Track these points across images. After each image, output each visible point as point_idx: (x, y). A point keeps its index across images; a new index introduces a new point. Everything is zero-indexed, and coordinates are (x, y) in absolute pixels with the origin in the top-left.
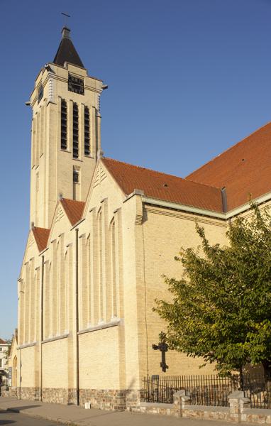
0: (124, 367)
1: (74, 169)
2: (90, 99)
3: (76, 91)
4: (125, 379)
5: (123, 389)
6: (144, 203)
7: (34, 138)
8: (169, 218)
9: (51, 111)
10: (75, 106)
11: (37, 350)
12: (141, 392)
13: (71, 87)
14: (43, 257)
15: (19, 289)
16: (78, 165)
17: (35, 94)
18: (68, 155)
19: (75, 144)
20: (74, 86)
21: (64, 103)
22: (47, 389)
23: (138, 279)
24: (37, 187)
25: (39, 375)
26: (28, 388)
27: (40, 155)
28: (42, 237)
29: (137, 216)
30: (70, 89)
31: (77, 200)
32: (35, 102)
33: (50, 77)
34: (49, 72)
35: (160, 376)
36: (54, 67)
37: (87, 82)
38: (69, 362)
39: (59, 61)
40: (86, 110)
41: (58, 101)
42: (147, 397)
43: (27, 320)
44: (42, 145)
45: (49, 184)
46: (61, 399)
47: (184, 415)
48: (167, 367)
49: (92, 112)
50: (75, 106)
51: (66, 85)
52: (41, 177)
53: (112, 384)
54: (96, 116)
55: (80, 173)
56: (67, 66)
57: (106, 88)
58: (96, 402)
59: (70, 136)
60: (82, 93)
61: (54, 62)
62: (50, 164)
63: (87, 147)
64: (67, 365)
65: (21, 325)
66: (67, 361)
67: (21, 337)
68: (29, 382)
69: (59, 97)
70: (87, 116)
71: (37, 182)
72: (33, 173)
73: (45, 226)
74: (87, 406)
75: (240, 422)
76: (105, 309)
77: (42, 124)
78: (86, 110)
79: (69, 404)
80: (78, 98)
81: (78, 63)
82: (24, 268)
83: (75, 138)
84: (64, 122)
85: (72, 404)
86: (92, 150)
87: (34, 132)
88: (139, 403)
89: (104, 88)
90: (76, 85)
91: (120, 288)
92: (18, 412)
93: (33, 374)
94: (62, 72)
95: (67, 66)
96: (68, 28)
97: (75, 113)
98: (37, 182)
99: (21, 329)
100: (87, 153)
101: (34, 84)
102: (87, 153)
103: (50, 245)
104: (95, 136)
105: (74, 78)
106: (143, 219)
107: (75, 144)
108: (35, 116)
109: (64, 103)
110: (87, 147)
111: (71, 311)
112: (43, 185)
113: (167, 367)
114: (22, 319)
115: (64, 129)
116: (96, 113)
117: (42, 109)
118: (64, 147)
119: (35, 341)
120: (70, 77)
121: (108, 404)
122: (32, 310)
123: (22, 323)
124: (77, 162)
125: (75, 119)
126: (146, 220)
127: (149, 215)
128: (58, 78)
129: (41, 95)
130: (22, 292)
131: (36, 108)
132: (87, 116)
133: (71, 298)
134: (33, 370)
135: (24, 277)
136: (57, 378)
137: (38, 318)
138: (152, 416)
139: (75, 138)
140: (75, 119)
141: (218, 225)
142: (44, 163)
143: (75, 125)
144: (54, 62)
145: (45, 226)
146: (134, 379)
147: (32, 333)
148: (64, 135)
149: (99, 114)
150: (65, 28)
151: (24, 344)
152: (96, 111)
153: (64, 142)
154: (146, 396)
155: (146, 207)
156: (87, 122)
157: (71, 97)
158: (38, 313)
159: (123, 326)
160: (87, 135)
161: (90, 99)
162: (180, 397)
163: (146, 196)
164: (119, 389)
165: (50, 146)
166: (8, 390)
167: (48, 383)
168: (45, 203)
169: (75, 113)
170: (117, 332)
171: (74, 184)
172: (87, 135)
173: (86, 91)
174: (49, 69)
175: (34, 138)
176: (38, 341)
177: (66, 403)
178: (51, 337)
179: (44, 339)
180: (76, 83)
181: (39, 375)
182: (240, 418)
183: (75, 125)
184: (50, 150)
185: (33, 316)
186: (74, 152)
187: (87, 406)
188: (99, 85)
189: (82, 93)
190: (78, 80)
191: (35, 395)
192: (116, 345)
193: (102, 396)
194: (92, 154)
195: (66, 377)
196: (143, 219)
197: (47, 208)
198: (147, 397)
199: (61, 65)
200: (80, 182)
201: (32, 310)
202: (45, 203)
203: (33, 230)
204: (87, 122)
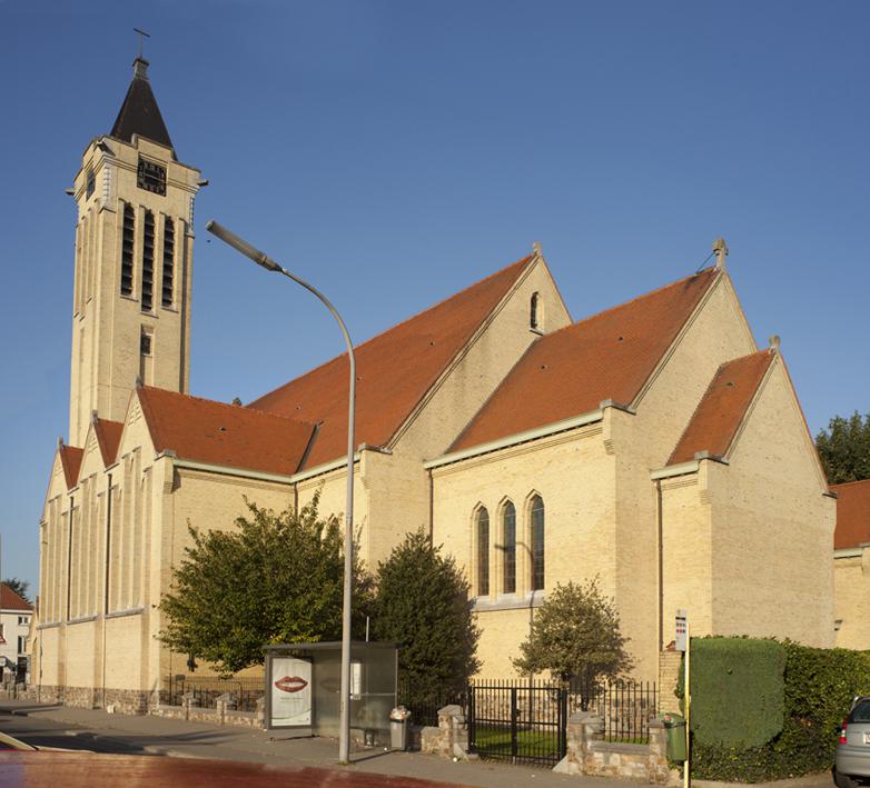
0: (147, 664)
1: (142, 330)
2: (175, 203)
3: (152, 187)
4: (147, 679)
5: (145, 689)
6: (175, 467)
7: (79, 261)
8: (210, 483)
9: (105, 224)
10: (149, 216)
11: (62, 634)
12: (160, 692)
13: (142, 180)
14: (72, 498)
15: (41, 540)
16: (151, 324)
17: (81, 180)
18: (133, 306)
19: (147, 286)
20: (148, 180)
21: (128, 210)
22: (72, 688)
23: (162, 556)
24: (81, 354)
25: (99, 668)
26: (50, 687)
27: (86, 300)
28: (72, 459)
29: (166, 483)
30: (140, 185)
31: (146, 383)
32: (82, 193)
33: (105, 161)
34: (104, 153)
35: (187, 676)
36: (113, 144)
37: (173, 172)
38: (96, 654)
39: (122, 132)
40: (169, 223)
41: (119, 207)
42: (170, 699)
43: (50, 587)
44: (90, 281)
45: (100, 355)
46: (85, 701)
47: (190, 718)
48: (196, 666)
49: (178, 228)
50: (149, 216)
51: (133, 177)
52: (88, 339)
53: (133, 684)
54: (186, 236)
55: (153, 337)
56: (137, 141)
57: (206, 184)
58: (119, 706)
59: (138, 270)
60: (162, 192)
61: (113, 134)
62: (102, 321)
63: (167, 292)
64: (93, 657)
65: (44, 593)
66: (93, 652)
67: (43, 610)
68: (51, 680)
69: (120, 199)
70: (169, 234)
71: (82, 344)
72: (77, 325)
73: (78, 441)
74: (110, 709)
75: (223, 723)
76: (131, 590)
77: (91, 243)
78: (169, 223)
79: (94, 708)
80: (155, 203)
81: (162, 138)
82: (48, 506)
83: (147, 274)
84: (128, 244)
85: (99, 708)
86: (176, 296)
87: (80, 250)
88: (158, 706)
89: (201, 185)
90: (152, 178)
91: (146, 567)
92: (25, 715)
93: (56, 666)
94: (126, 153)
95: (137, 141)
96: (144, 58)
97: (149, 228)
98: (82, 344)
99: (44, 599)
100: (167, 302)
101: (82, 161)
102: (167, 302)
103: (80, 485)
104: (181, 271)
105: (149, 164)
106: (175, 485)
107: (147, 286)
108: (81, 221)
109: (128, 210)
110: (167, 292)
111: (100, 585)
112: (90, 355)
113: (196, 666)
114: (43, 584)
115: (127, 257)
116: (186, 230)
117: (92, 214)
118: (126, 289)
119: (96, 614)
120: (141, 162)
121: (130, 707)
122: (57, 575)
123: (44, 589)
124: (148, 318)
125: (149, 239)
126: (179, 486)
127: (183, 481)
128: (120, 165)
129: (91, 187)
130: (45, 543)
131: (85, 206)
132: (169, 234)
133: (101, 569)
134: (56, 662)
135: (47, 519)
136: (80, 677)
137: (64, 585)
138: (166, 719)
139: (147, 274)
140: (149, 239)
141: (281, 490)
142: (92, 313)
143: (148, 251)
144: (113, 134)
145: (78, 441)
146: (154, 682)
147: (57, 608)
148: (127, 268)
149: (191, 232)
150: (138, 60)
151: (47, 623)
152: (186, 225)
153: (126, 281)
154: (167, 698)
155: (179, 470)
156: (169, 245)
157: (143, 199)
158: (64, 578)
159: (148, 615)
160: (168, 268)
161: (175, 203)
162: (188, 698)
163: (179, 457)
164: (139, 689)
165: (102, 288)
166: (25, 689)
167: (73, 681)
168: (92, 387)
169: (149, 228)
170: (140, 622)
171: (142, 358)
172: (168, 268)
173: (168, 188)
174: (104, 147)
175: (79, 259)
176: (62, 620)
177: (91, 706)
178: (78, 617)
179: (110, 612)
180: (151, 173)
181: (99, 668)
182: (223, 719)
183: (148, 251)
184: (102, 295)
185: (57, 586)
186: (143, 299)
187: (110, 709)
188: (192, 177)
189: (162, 192)
190: (156, 167)
191: (58, 697)
192: (139, 637)
193: (125, 697)
194: (176, 305)
195: (92, 673)
196: (175, 485)
197: (95, 398)
198: (170, 699)
199: (126, 139)
200: (152, 354)
201: (57, 575)
202: (92, 387)
203: (61, 450)
204: (169, 245)
